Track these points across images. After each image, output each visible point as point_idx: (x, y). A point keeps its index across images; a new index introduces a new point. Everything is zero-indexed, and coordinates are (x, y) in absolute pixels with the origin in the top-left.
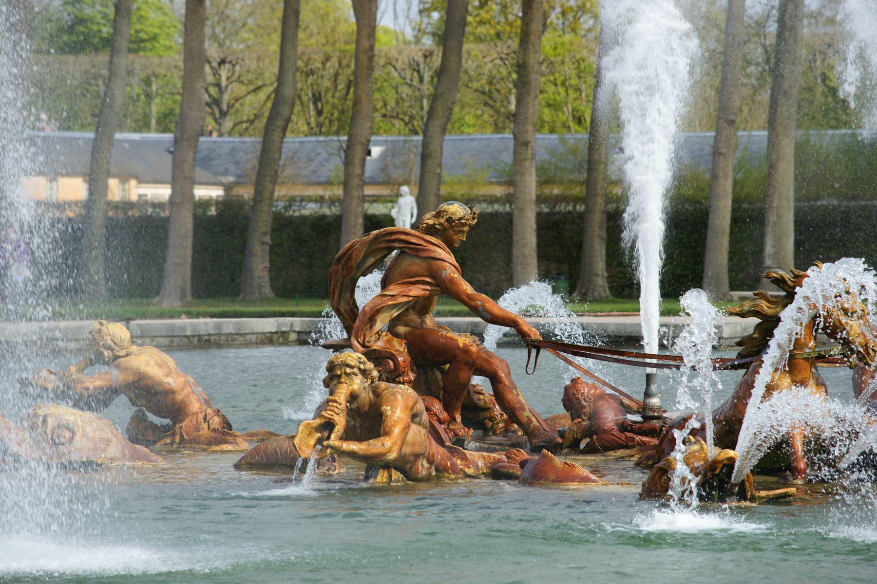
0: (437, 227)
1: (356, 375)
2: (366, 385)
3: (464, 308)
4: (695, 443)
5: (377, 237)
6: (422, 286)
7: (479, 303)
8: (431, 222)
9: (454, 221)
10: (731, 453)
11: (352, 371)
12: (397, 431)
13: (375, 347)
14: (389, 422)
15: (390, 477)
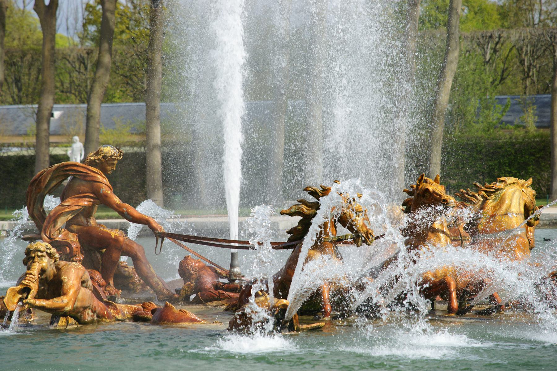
0: (97, 161)
1: (44, 257)
2: (51, 263)
3: (116, 214)
4: (262, 296)
5: (58, 168)
6: (87, 199)
7: (125, 209)
8: (92, 158)
9: (107, 157)
10: (284, 301)
11: (42, 254)
12: (71, 292)
13: (57, 239)
14: (66, 287)
15: (67, 322)
